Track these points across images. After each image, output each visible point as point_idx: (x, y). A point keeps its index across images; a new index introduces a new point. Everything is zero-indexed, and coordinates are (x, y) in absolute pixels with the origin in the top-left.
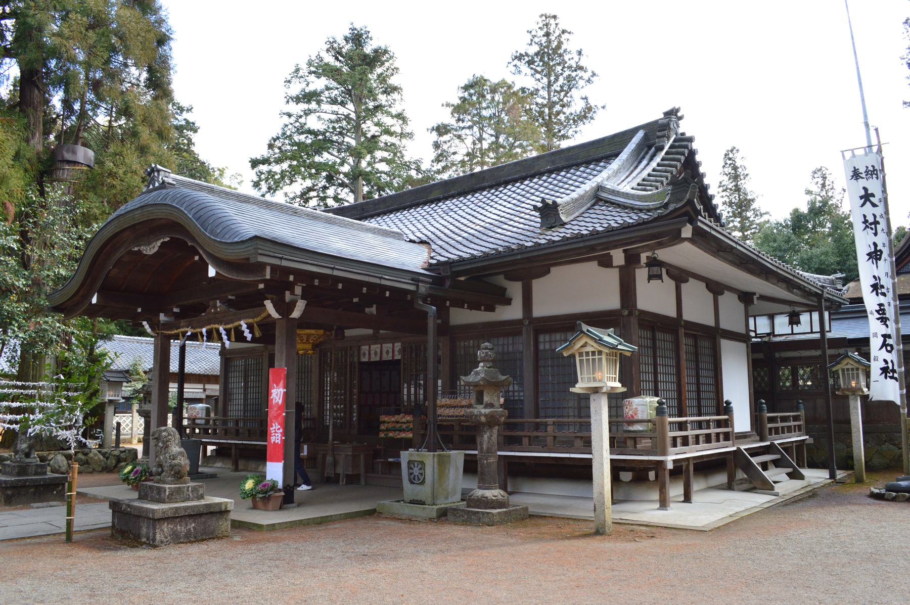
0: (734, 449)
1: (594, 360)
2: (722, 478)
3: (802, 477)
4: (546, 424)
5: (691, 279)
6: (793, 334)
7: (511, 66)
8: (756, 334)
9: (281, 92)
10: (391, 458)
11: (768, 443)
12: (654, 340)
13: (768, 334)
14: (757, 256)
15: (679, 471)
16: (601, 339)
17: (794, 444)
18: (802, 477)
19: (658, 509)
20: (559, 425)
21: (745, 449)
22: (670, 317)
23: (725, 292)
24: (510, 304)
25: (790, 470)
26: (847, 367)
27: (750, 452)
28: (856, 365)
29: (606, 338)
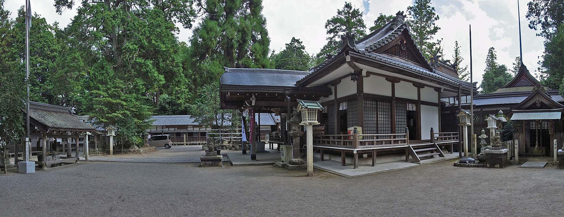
0: (408, 146)
1: (464, 118)
2: (404, 158)
3: (443, 156)
4: (330, 137)
5: (401, 81)
6: (466, 103)
7: (408, 12)
8: (450, 104)
9: (326, 30)
10: (558, 142)
11: (433, 144)
12: (377, 105)
13: (453, 104)
14: (385, 63)
15: (361, 154)
16: (465, 112)
17: (453, 144)
18: (443, 156)
19: (353, 168)
20: (334, 137)
21: (412, 147)
22: (385, 96)
23: (425, 87)
24: (332, 94)
25: (440, 153)
26: (462, 115)
27: (414, 148)
28: (465, 115)
29: (467, 112)
